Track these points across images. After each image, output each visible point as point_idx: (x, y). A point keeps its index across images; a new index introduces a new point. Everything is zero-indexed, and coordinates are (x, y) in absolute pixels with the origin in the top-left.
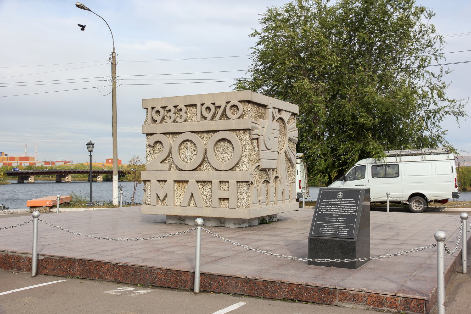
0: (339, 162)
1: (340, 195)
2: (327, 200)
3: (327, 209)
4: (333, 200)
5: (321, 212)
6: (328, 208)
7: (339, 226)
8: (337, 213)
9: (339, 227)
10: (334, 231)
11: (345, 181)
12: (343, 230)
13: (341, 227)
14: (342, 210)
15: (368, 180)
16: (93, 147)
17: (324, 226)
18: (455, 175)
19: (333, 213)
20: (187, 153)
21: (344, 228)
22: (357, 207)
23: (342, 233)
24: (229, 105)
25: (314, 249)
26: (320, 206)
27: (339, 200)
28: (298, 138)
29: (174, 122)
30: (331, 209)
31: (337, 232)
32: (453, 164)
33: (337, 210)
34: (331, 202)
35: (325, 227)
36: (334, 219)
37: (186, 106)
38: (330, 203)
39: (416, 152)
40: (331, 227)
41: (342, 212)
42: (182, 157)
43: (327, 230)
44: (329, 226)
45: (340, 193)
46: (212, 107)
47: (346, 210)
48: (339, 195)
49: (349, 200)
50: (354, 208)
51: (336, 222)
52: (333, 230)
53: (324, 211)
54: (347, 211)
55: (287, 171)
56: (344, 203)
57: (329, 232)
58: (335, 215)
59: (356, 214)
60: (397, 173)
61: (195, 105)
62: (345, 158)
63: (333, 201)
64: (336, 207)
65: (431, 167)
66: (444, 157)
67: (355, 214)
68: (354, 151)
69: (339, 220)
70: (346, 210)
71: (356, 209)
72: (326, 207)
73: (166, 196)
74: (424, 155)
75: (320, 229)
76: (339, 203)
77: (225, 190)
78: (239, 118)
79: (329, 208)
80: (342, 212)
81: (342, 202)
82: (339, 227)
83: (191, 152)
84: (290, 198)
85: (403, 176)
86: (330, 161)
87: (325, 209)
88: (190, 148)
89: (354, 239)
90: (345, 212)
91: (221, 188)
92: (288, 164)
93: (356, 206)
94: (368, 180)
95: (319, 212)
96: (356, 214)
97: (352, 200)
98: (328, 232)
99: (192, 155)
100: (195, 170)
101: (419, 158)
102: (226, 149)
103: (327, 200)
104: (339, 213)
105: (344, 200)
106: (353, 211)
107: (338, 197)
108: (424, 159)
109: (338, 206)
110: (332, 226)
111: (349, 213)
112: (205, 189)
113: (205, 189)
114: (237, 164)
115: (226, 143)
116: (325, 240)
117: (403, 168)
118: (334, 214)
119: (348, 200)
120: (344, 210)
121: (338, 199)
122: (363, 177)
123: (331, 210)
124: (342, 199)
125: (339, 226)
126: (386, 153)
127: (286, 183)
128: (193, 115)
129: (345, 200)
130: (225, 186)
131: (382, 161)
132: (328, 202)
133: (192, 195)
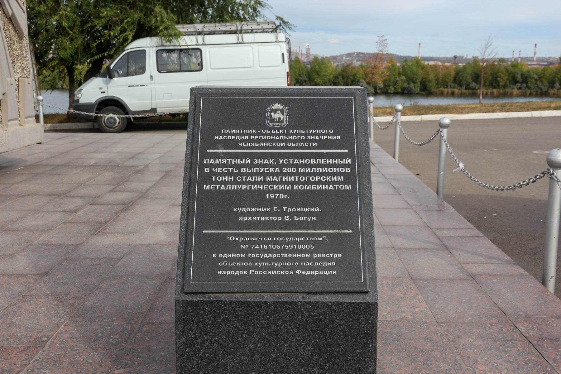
0: (101, 42)
4: (254, 134)
5: (212, 187)
6: (239, 167)
8: (282, 187)
9: (300, 247)
10: (280, 264)
11: (111, 77)
14: (298, 174)
15: (151, 76)
17: (234, 247)
18: (286, 68)
21: (319, 247)
22: (353, 161)
23: (316, 273)
25: (202, 346)
27: (279, 135)
31: (294, 268)
32: (284, 48)
33: (277, 174)
34: (248, 144)
35: (243, 251)
36: (271, 214)
38: (243, 148)
39: (228, 28)
41: (299, 183)
43: (253, 260)
44: (256, 243)
45: (277, 106)
47: (315, 174)
48: (274, 116)
49: (315, 134)
50: (345, 166)
51: (283, 225)
52: (277, 260)
53: (225, 183)
54: (318, 178)
55: (7, 49)
56: (298, 144)
57: (263, 268)
59: (354, 187)
60: (199, 64)
62: (110, 35)
63: (253, 141)
64: (271, 161)
65: (251, 55)
66: (270, 37)
67: (349, 187)
68: (126, 23)
70: (315, 174)
71: (352, 166)
72: (232, 165)
74: (241, 33)
75: (222, 260)
79: (245, 166)
80: (299, 183)
81: (292, 141)
82: (300, 247)
84: (22, 115)
85: (209, 69)
86: (79, 41)
89: (367, 292)
90: (309, 183)
92: (8, 29)
93: (350, 155)
94: (151, 76)
95: (206, 187)
96: (354, 187)
97: (328, 134)
98: (256, 268)
101: (232, 38)
103: (231, 134)
105: (297, 134)
106: (342, 179)
107: (273, 120)
108: (240, 41)
110: (272, 242)
111: (329, 183)
116: (246, 304)
117: (208, 56)
119: (312, 134)
120: (304, 174)
121: (275, 129)
122: (142, 70)
123: (252, 174)
126: (180, 28)
127: (9, 79)
129: (301, 134)
131: (175, 42)
132: (234, 144)
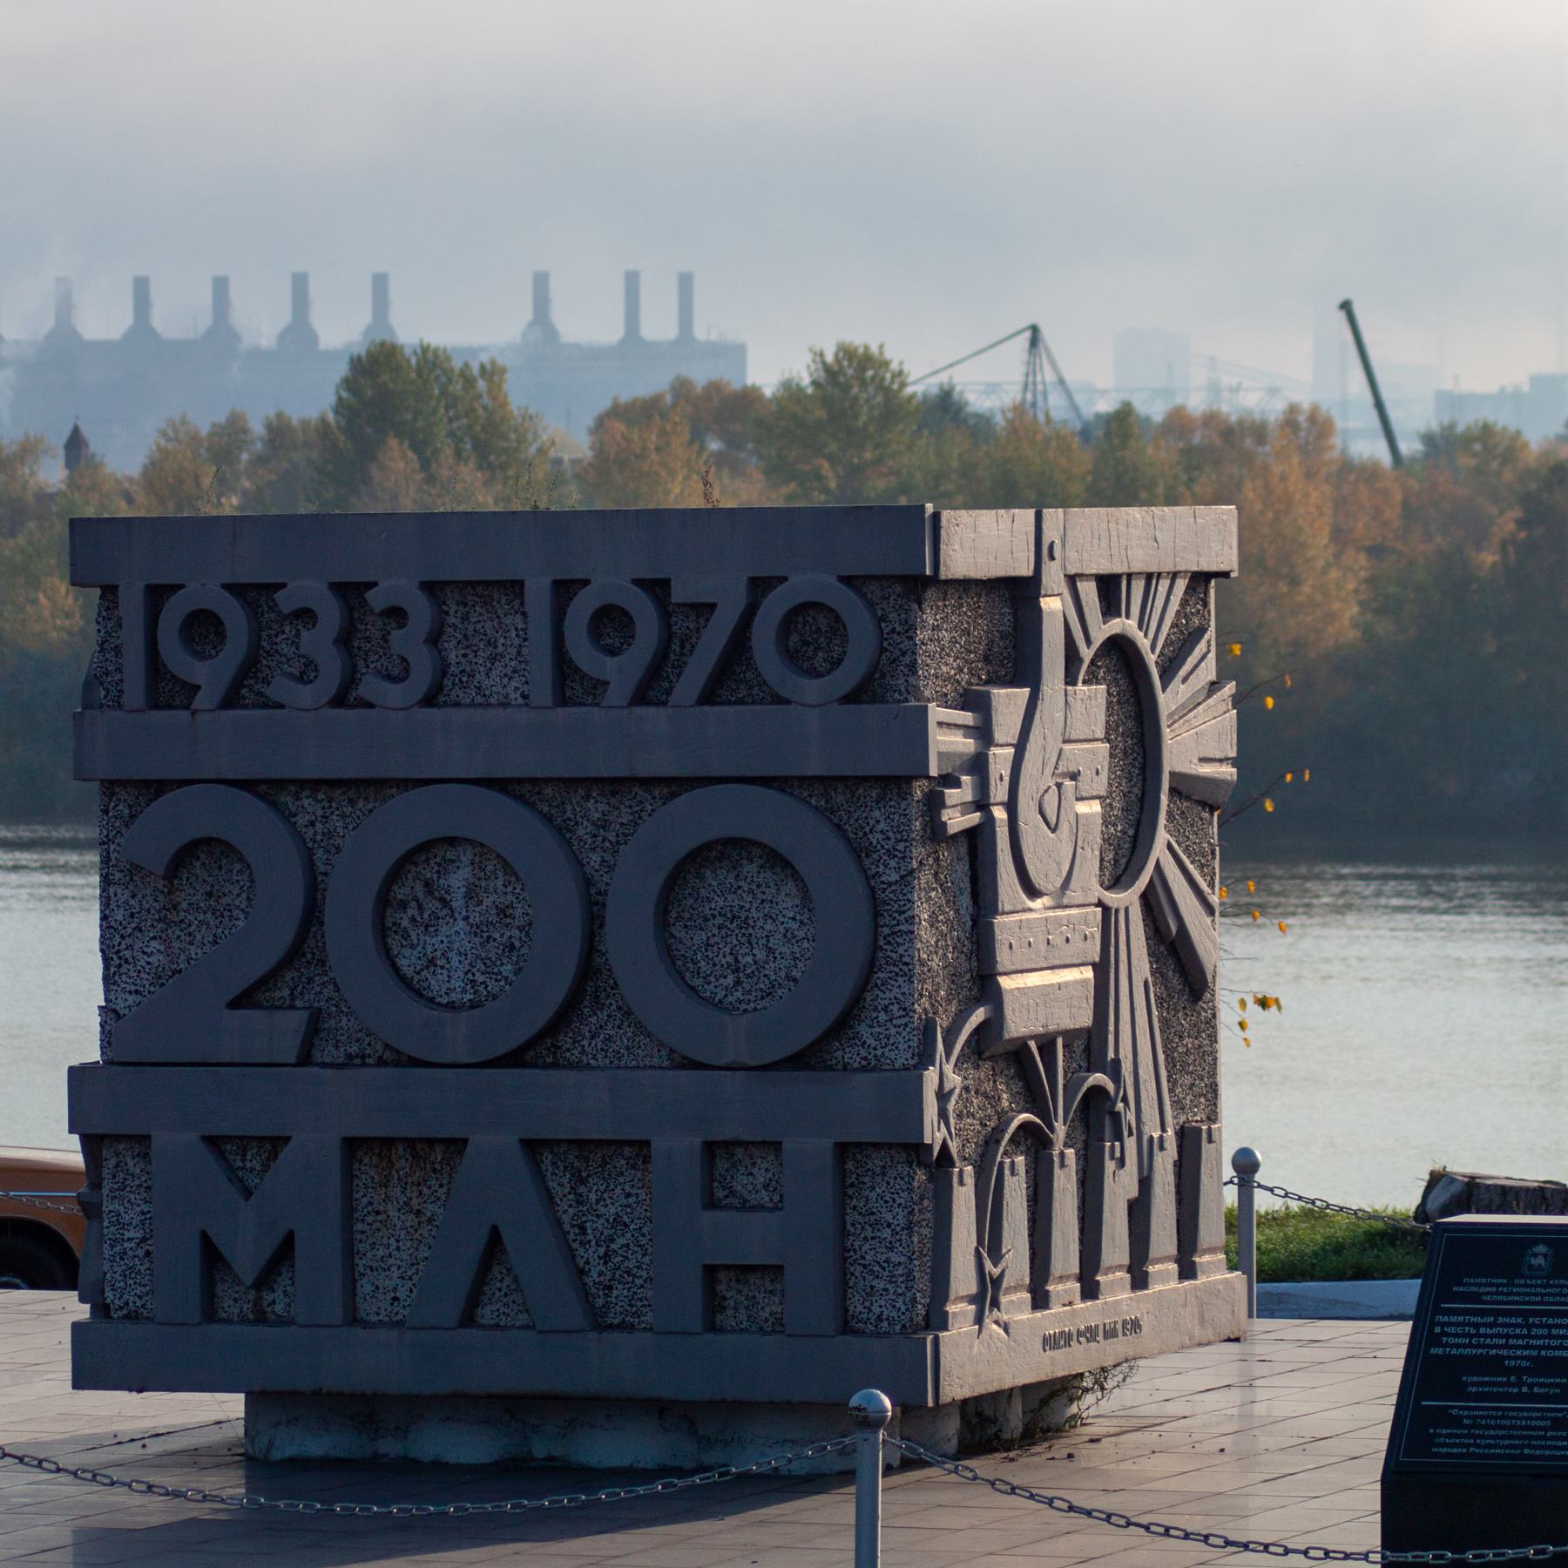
1: (1539, 1257)
2: (1473, 1284)
3: (1473, 1331)
5: (1440, 1351)
6: (1477, 1326)
7: (1531, 1418)
8: (1526, 1353)
10: (1506, 1442)
12: (1552, 1438)
13: (1543, 1423)
14: (1549, 1336)
16: (410, 1057)
19: (1505, 1352)
20: (444, 930)
23: (1548, 1453)
24: (775, 606)
26: (1439, 1318)
27: (1536, 1286)
28: (1235, 762)
29: (339, 701)
30: (1495, 1331)
31: (1522, 1447)
35: (1466, 1427)
36: (1508, 1384)
37: (431, 588)
40: (1493, 1422)
41: (1549, 1347)
42: (408, 962)
43: (1476, 1437)
45: (1541, 1249)
46: (642, 609)
48: (1534, 1261)
52: (1503, 1437)
53: (1458, 1346)
58: (1513, 1363)
61: (515, 588)
63: (1502, 1293)
64: (1519, 1320)
69: (1536, 1390)
73: (285, 1250)
75: (1440, 1435)
76: (1533, 1299)
77: (746, 1207)
78: (851, 698)
80: (1549, 1347)
81: (1549, 1295)
82: (1534, 1423)
83: (475, 930)
87: (1464, 1335)
88: (469, 895)
91: (720, 1193)
95: (1433, 1351)
98: (1479, 1446)
99: (493, 950)
100: (514, 1059)
102: (754, 913)
104: (1534, 1353)
107: (1531, 1267)
109: (1526, 1314)
112: (593, 1197)
113: (593, 1197)
114: (843, 1025)
115: (714, 879)
118: (1509, 1358)
123: (1492, 1336)
124: (1548, 1277)
125: (1531, 1418)
128: (493, 659)
130: (745, 1180)
132: (1476, 1298)
133: (495, 1236)
